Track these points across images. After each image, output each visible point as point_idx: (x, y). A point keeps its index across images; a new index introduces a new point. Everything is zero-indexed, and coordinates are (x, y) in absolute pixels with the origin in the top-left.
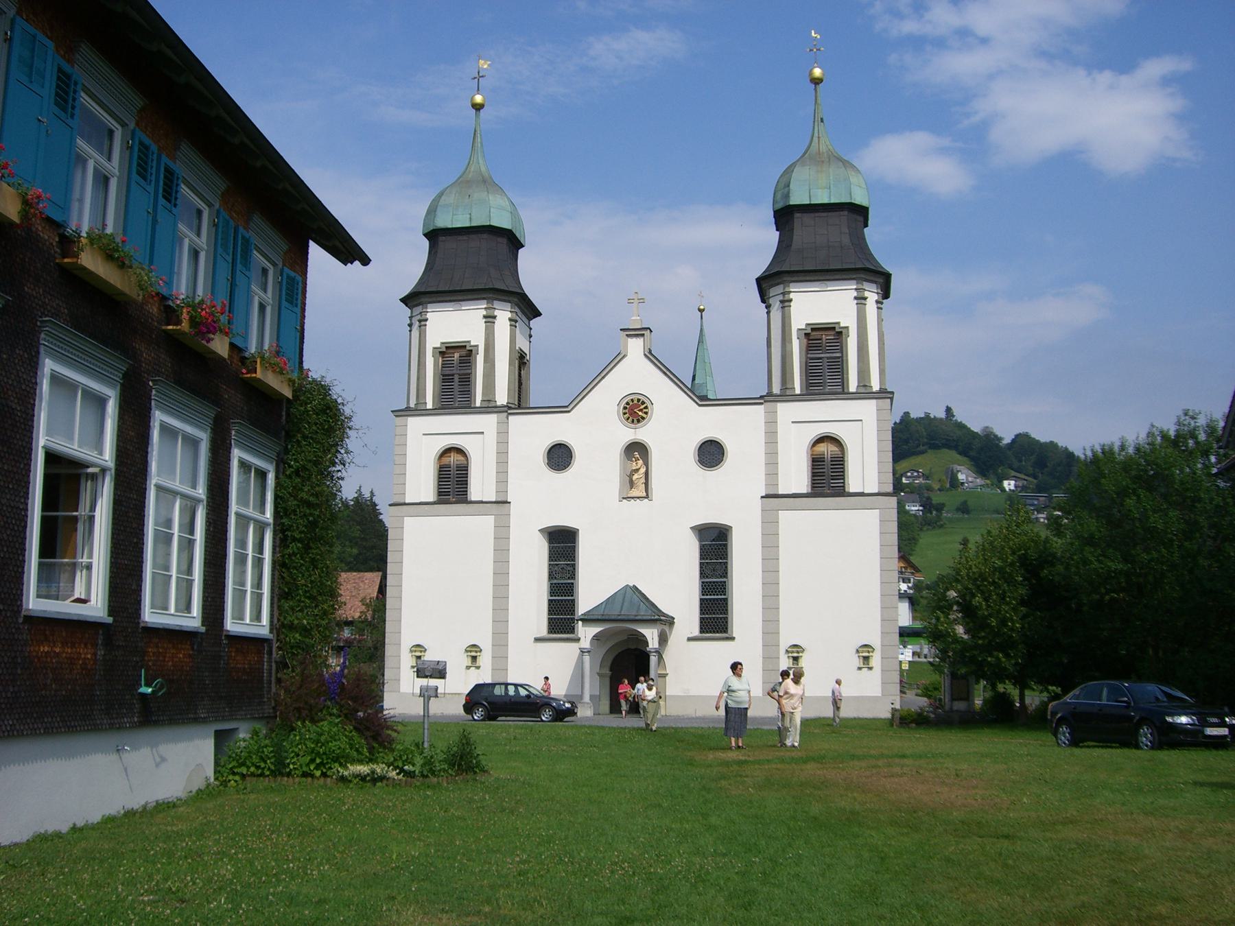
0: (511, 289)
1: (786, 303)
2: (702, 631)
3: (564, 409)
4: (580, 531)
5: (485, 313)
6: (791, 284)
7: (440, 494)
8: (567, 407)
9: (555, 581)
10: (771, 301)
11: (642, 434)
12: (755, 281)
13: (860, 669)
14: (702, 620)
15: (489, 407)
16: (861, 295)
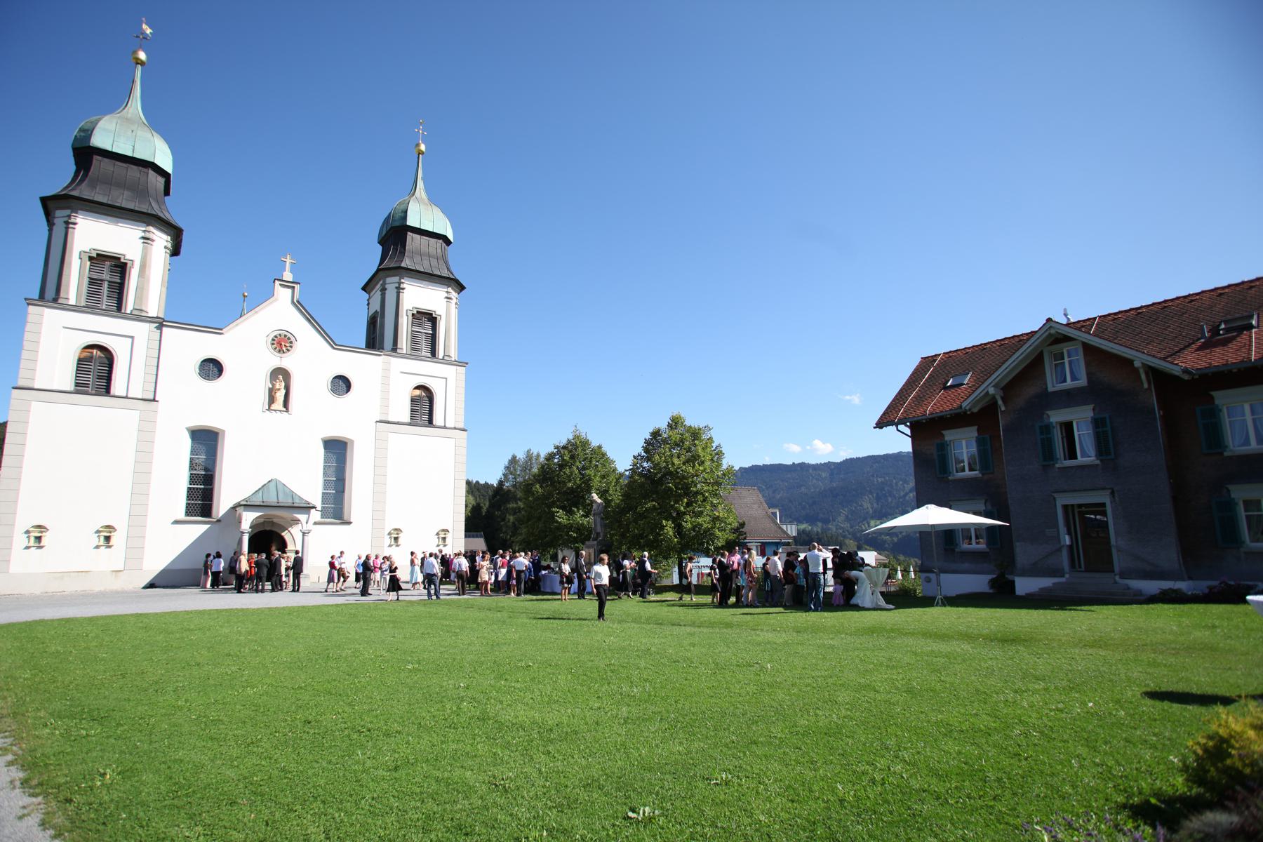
0: (443, 275)
1: (68, 224)
2: (188, 513)
3: (217, 330)
4: (227, 434)
5: (143, 234)
6: (405, 278)
7: (77, 385)
8: (336, 345)
9: (195, 472)
10: (56, 221)
11: (286, 362)
12: (183, 228)
13: (97, 547)
14: (188, 505)
15: (139, 316)
16: (449, 296)
